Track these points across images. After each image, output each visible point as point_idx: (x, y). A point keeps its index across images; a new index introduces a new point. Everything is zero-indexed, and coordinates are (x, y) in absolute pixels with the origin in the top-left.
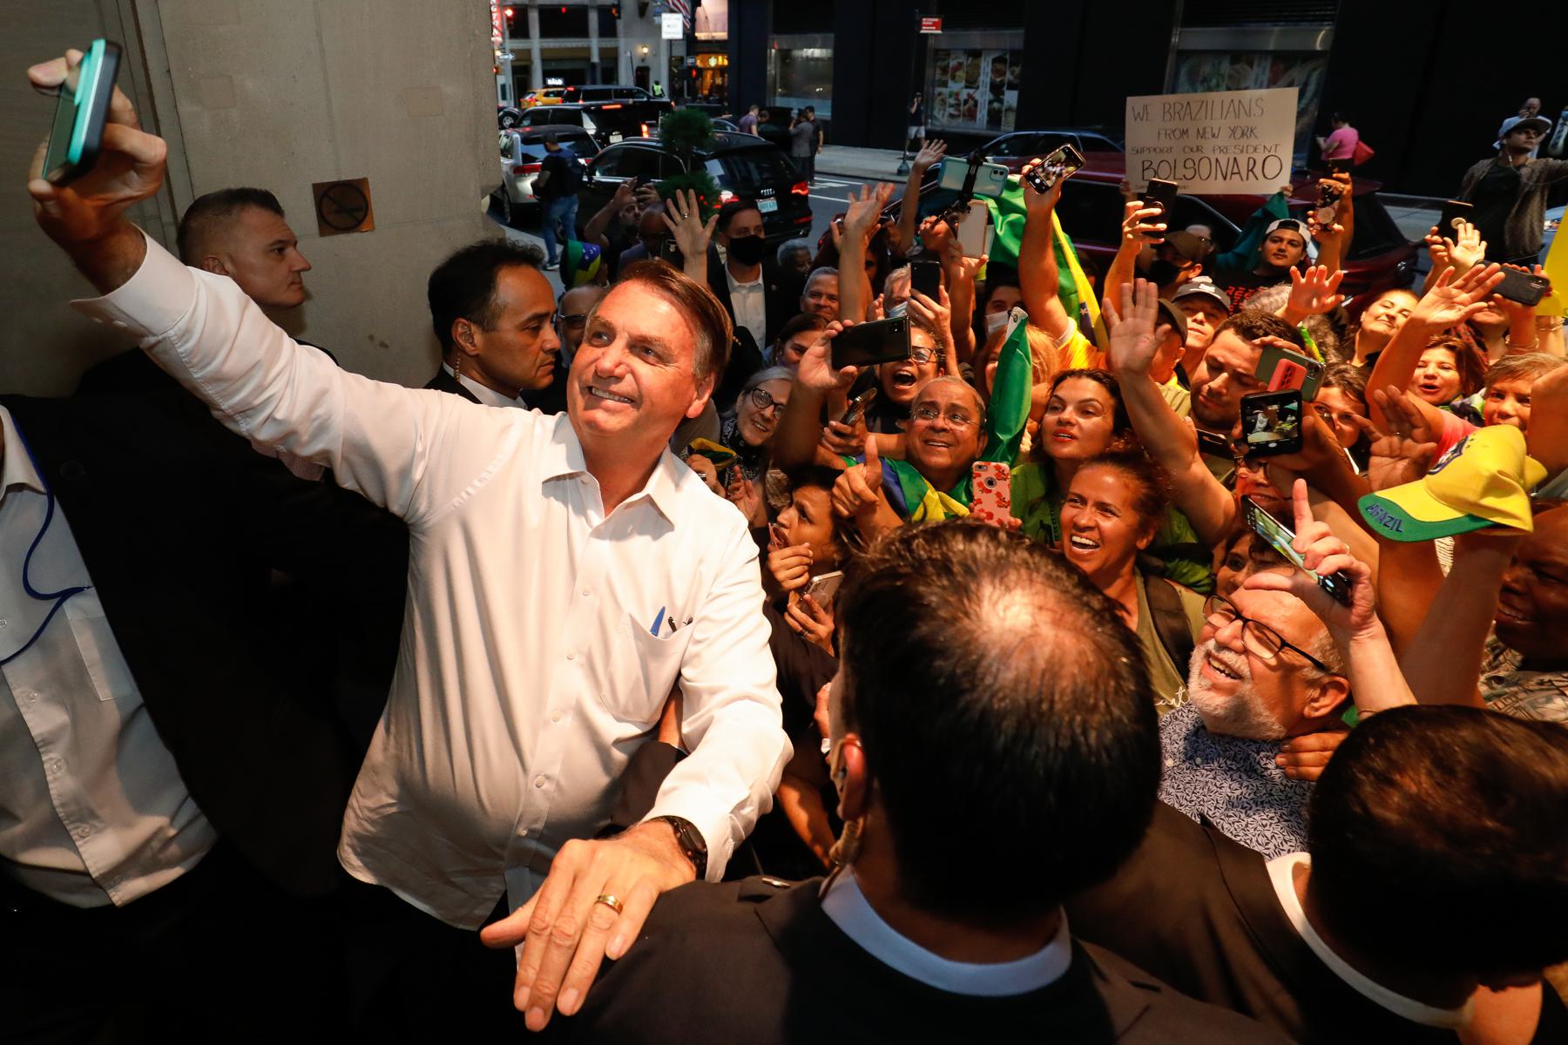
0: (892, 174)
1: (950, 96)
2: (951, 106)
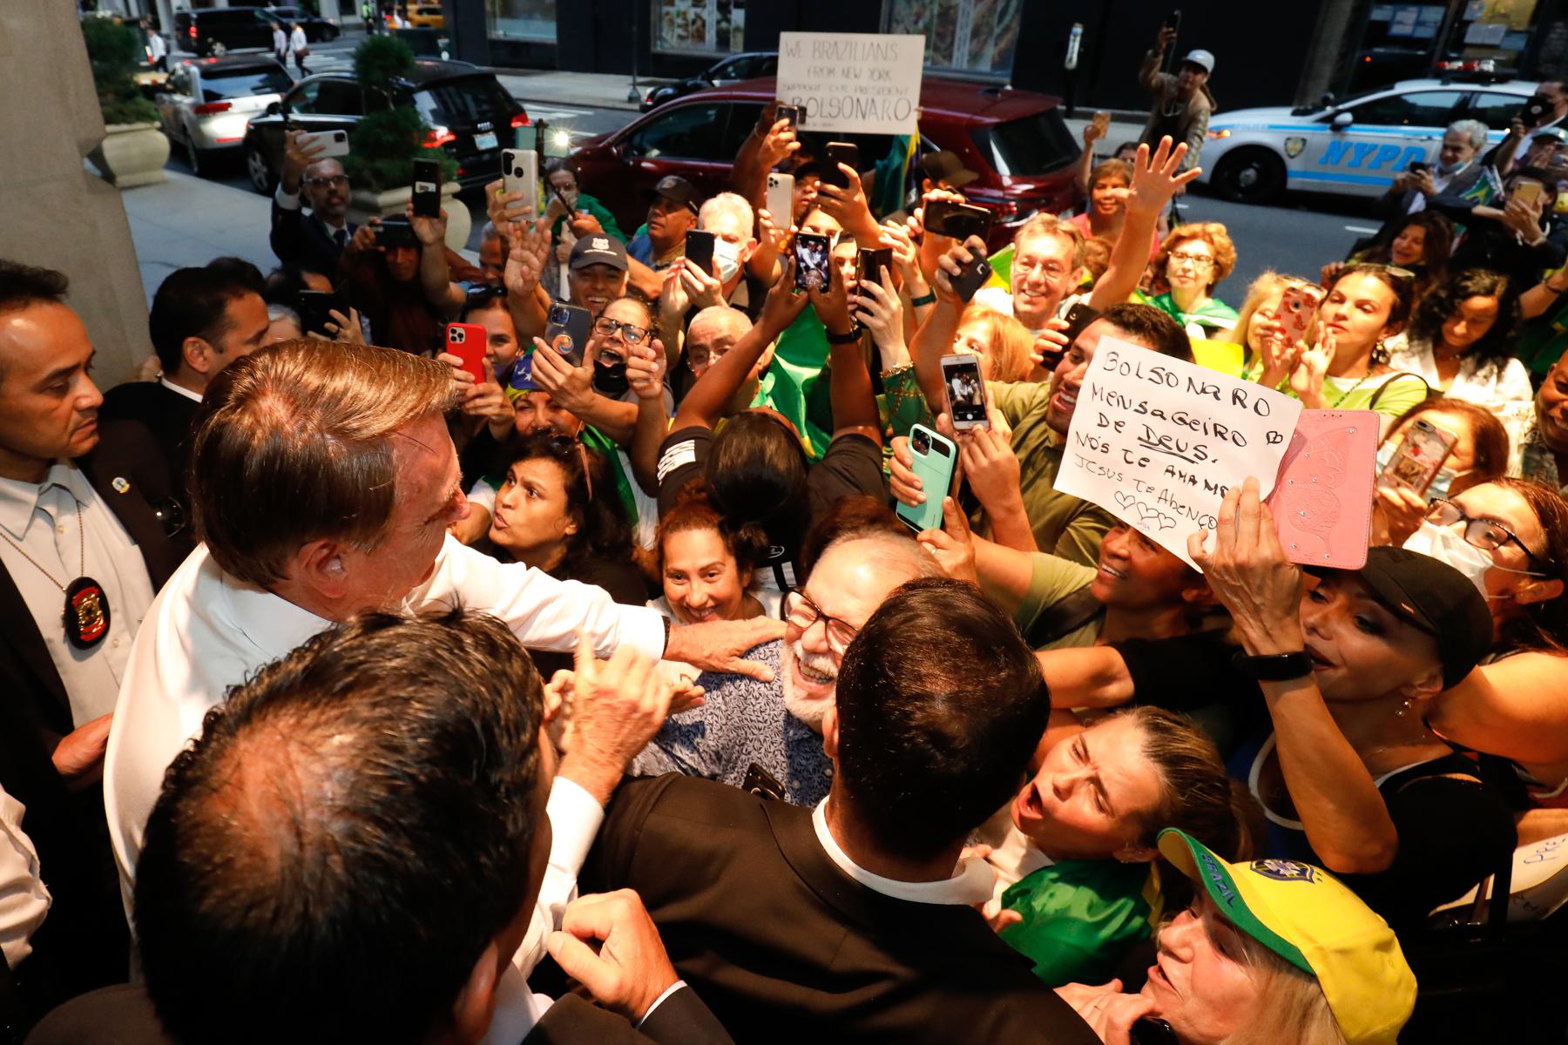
0: (623, 102)
1: (678, 15)
2: (679, 26)
